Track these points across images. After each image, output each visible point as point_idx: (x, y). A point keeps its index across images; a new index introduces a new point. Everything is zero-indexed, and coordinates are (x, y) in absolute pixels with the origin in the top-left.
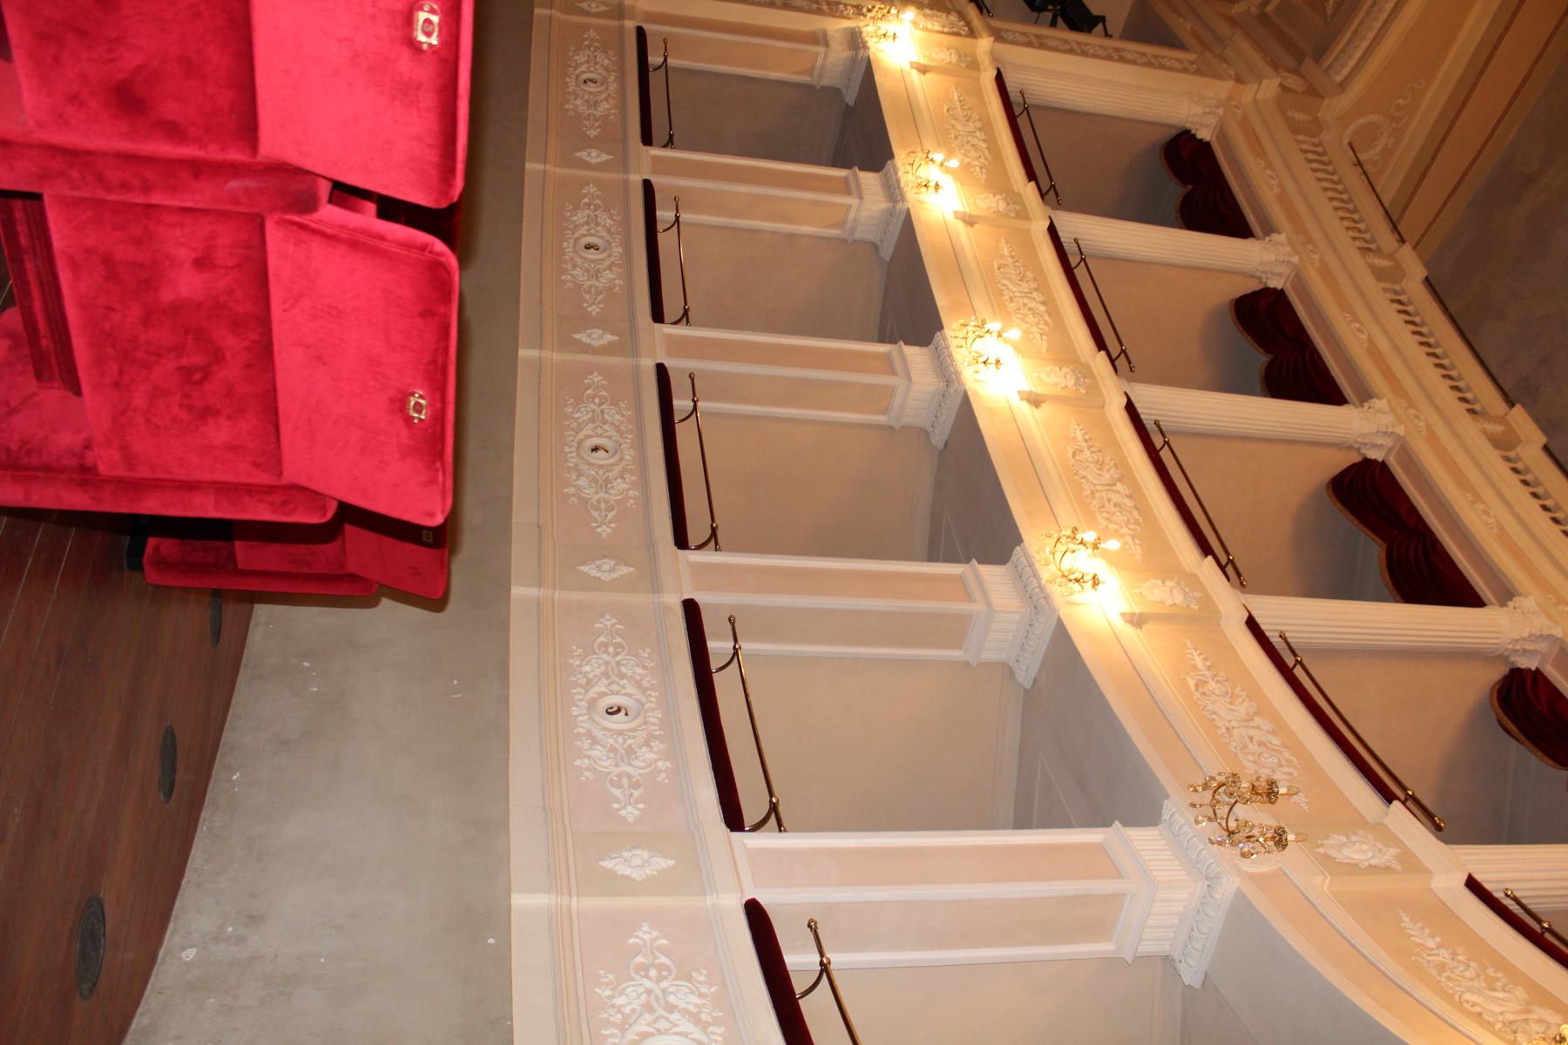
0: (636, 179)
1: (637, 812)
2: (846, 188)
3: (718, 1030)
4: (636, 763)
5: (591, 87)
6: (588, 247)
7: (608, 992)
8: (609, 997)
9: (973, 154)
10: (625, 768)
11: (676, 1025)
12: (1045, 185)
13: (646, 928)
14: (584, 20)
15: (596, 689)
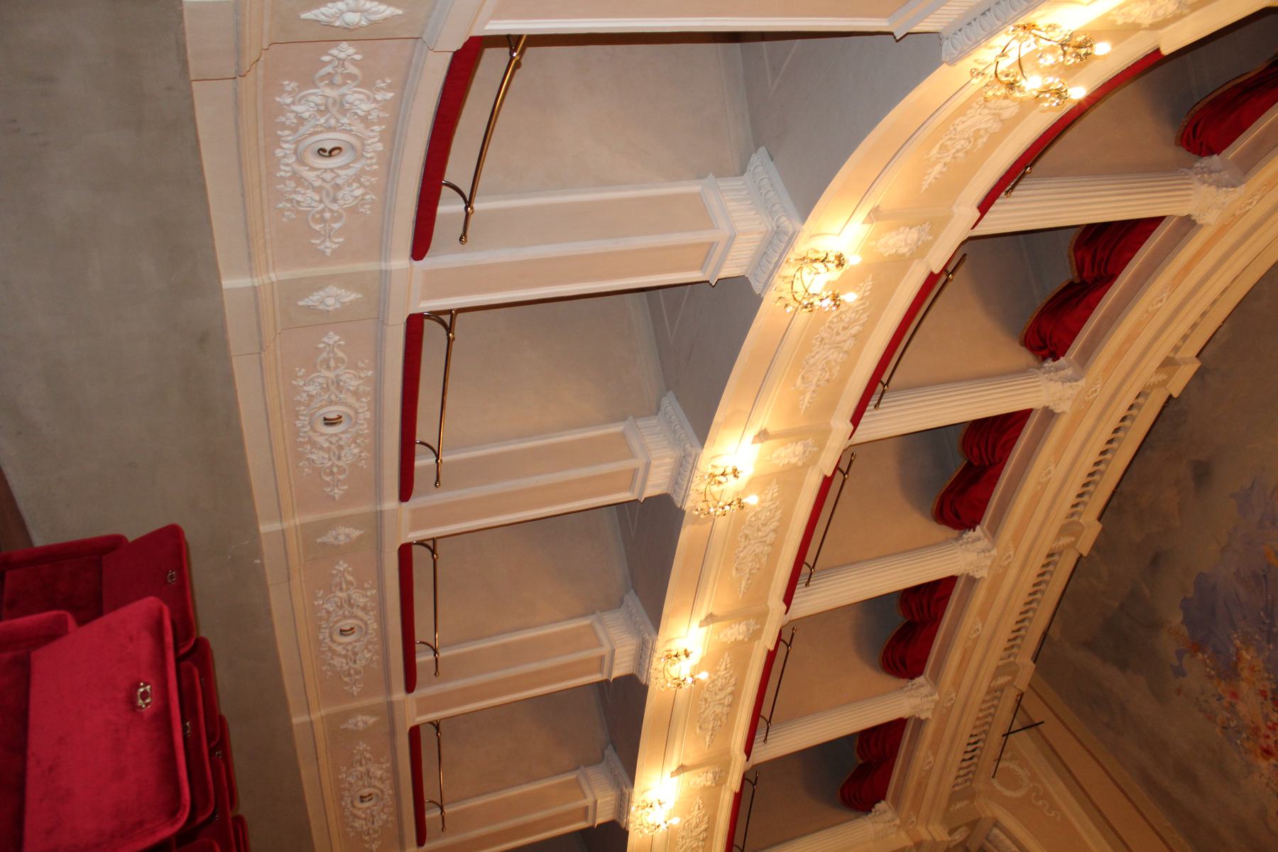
1: (325, 339)
3: (282, 174)
4: (318, 100)
7: (367, 197)
8: (366, 194)
11: (318, 176)
13: (328, 251)
14: (365, 702)
15: (351, 172)
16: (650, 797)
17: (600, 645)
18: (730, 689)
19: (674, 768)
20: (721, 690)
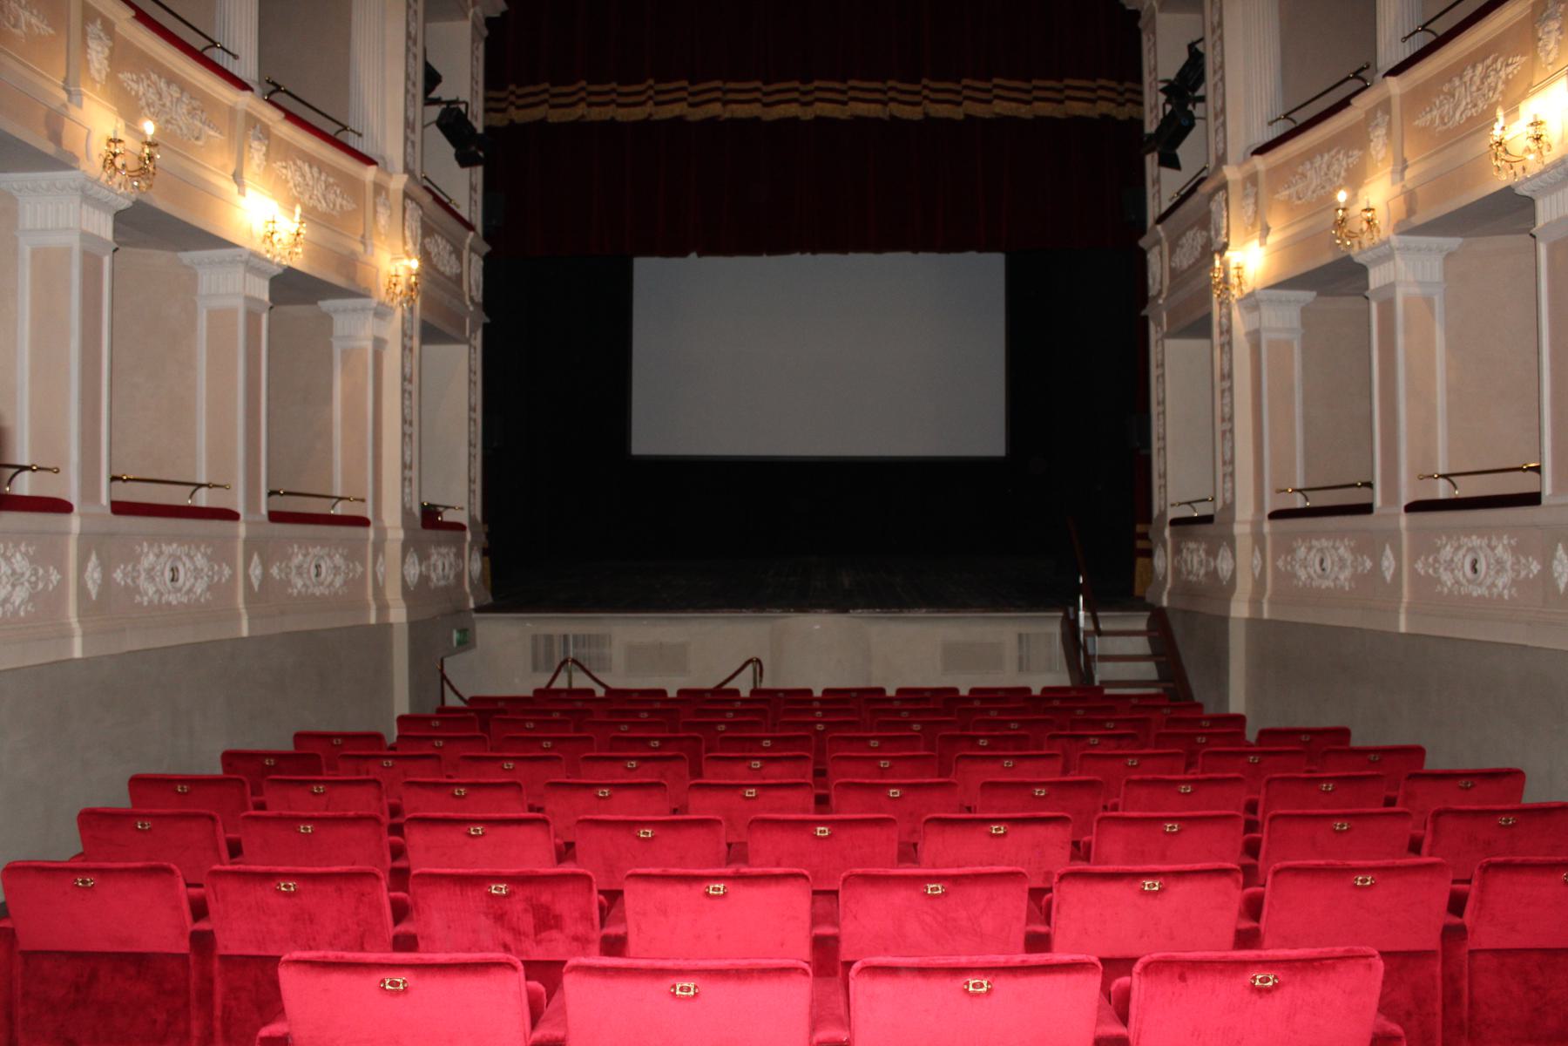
0: (1404, 520)
2: (1388, 306)
5: (1328, 564)
6: (1474, 570)
9: (1335, 167)
10: (1509, 564)
12: (1354, 85)
16: (260, 230)
17: (68, 250)
18: (163, 85)
19: (235, 188)
20: (161, 98)
